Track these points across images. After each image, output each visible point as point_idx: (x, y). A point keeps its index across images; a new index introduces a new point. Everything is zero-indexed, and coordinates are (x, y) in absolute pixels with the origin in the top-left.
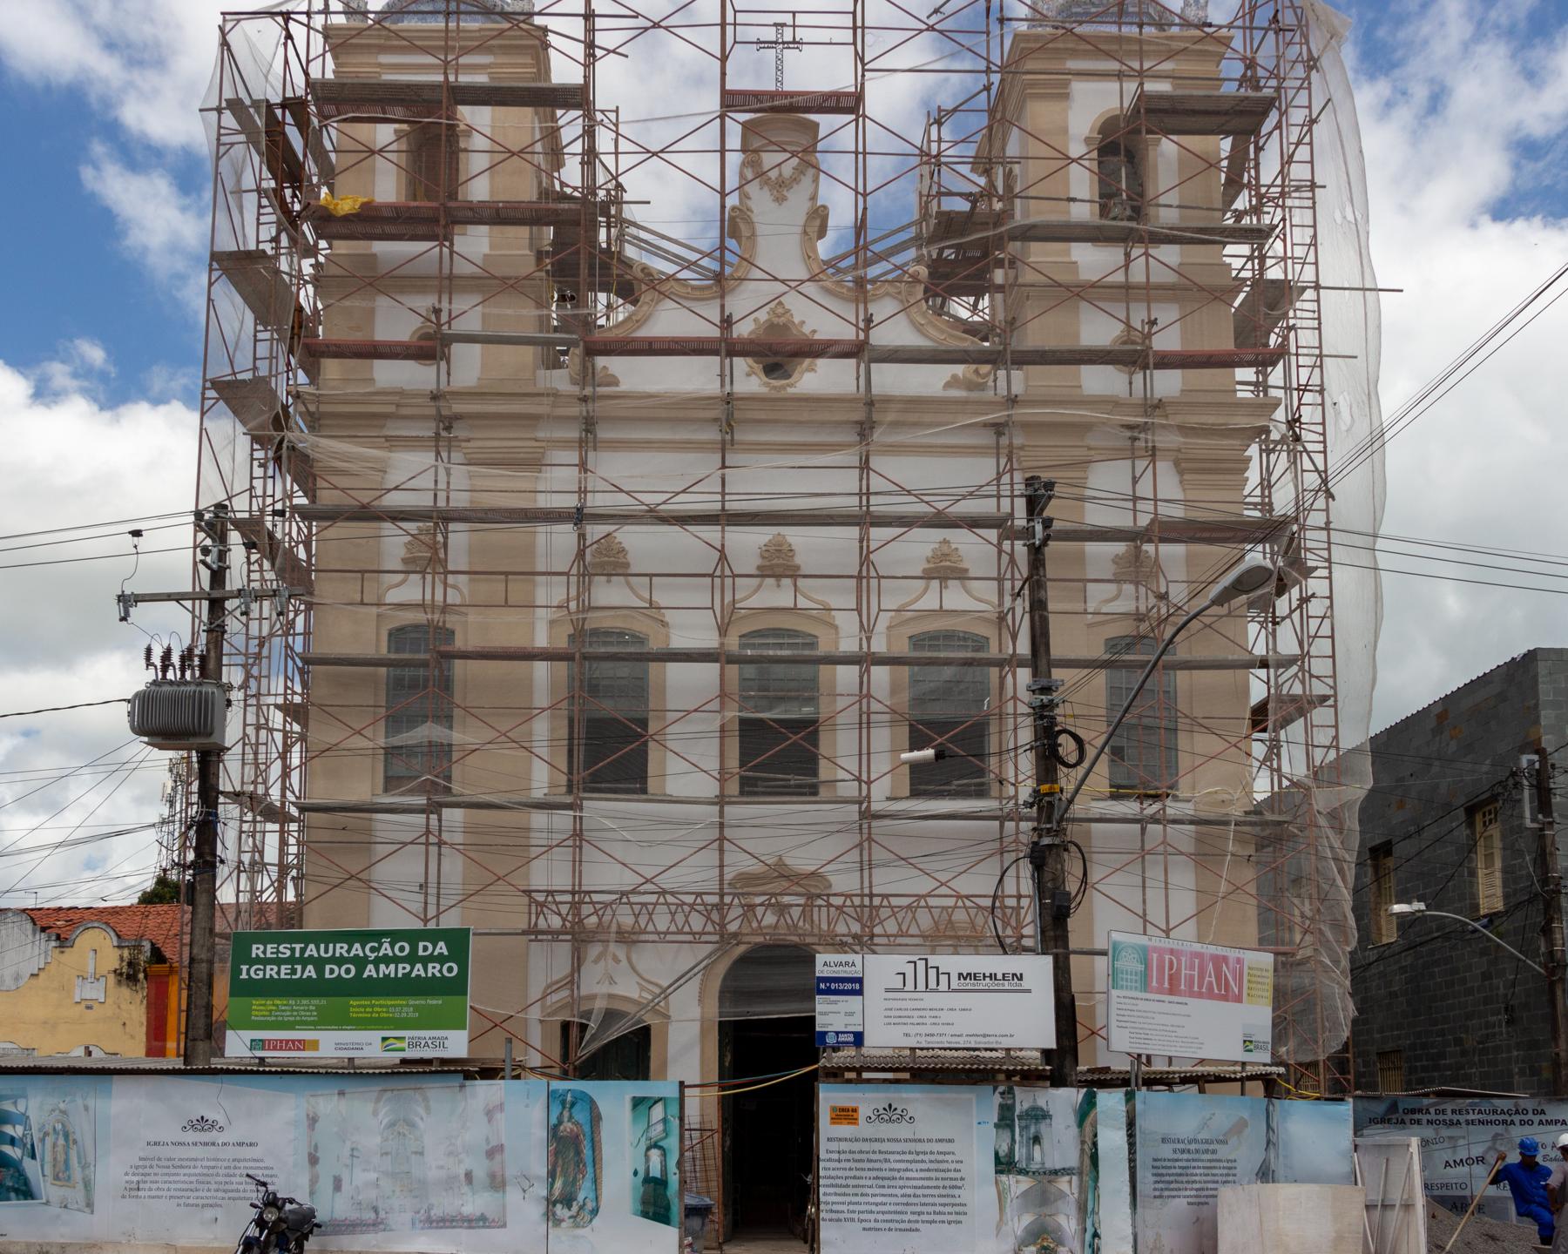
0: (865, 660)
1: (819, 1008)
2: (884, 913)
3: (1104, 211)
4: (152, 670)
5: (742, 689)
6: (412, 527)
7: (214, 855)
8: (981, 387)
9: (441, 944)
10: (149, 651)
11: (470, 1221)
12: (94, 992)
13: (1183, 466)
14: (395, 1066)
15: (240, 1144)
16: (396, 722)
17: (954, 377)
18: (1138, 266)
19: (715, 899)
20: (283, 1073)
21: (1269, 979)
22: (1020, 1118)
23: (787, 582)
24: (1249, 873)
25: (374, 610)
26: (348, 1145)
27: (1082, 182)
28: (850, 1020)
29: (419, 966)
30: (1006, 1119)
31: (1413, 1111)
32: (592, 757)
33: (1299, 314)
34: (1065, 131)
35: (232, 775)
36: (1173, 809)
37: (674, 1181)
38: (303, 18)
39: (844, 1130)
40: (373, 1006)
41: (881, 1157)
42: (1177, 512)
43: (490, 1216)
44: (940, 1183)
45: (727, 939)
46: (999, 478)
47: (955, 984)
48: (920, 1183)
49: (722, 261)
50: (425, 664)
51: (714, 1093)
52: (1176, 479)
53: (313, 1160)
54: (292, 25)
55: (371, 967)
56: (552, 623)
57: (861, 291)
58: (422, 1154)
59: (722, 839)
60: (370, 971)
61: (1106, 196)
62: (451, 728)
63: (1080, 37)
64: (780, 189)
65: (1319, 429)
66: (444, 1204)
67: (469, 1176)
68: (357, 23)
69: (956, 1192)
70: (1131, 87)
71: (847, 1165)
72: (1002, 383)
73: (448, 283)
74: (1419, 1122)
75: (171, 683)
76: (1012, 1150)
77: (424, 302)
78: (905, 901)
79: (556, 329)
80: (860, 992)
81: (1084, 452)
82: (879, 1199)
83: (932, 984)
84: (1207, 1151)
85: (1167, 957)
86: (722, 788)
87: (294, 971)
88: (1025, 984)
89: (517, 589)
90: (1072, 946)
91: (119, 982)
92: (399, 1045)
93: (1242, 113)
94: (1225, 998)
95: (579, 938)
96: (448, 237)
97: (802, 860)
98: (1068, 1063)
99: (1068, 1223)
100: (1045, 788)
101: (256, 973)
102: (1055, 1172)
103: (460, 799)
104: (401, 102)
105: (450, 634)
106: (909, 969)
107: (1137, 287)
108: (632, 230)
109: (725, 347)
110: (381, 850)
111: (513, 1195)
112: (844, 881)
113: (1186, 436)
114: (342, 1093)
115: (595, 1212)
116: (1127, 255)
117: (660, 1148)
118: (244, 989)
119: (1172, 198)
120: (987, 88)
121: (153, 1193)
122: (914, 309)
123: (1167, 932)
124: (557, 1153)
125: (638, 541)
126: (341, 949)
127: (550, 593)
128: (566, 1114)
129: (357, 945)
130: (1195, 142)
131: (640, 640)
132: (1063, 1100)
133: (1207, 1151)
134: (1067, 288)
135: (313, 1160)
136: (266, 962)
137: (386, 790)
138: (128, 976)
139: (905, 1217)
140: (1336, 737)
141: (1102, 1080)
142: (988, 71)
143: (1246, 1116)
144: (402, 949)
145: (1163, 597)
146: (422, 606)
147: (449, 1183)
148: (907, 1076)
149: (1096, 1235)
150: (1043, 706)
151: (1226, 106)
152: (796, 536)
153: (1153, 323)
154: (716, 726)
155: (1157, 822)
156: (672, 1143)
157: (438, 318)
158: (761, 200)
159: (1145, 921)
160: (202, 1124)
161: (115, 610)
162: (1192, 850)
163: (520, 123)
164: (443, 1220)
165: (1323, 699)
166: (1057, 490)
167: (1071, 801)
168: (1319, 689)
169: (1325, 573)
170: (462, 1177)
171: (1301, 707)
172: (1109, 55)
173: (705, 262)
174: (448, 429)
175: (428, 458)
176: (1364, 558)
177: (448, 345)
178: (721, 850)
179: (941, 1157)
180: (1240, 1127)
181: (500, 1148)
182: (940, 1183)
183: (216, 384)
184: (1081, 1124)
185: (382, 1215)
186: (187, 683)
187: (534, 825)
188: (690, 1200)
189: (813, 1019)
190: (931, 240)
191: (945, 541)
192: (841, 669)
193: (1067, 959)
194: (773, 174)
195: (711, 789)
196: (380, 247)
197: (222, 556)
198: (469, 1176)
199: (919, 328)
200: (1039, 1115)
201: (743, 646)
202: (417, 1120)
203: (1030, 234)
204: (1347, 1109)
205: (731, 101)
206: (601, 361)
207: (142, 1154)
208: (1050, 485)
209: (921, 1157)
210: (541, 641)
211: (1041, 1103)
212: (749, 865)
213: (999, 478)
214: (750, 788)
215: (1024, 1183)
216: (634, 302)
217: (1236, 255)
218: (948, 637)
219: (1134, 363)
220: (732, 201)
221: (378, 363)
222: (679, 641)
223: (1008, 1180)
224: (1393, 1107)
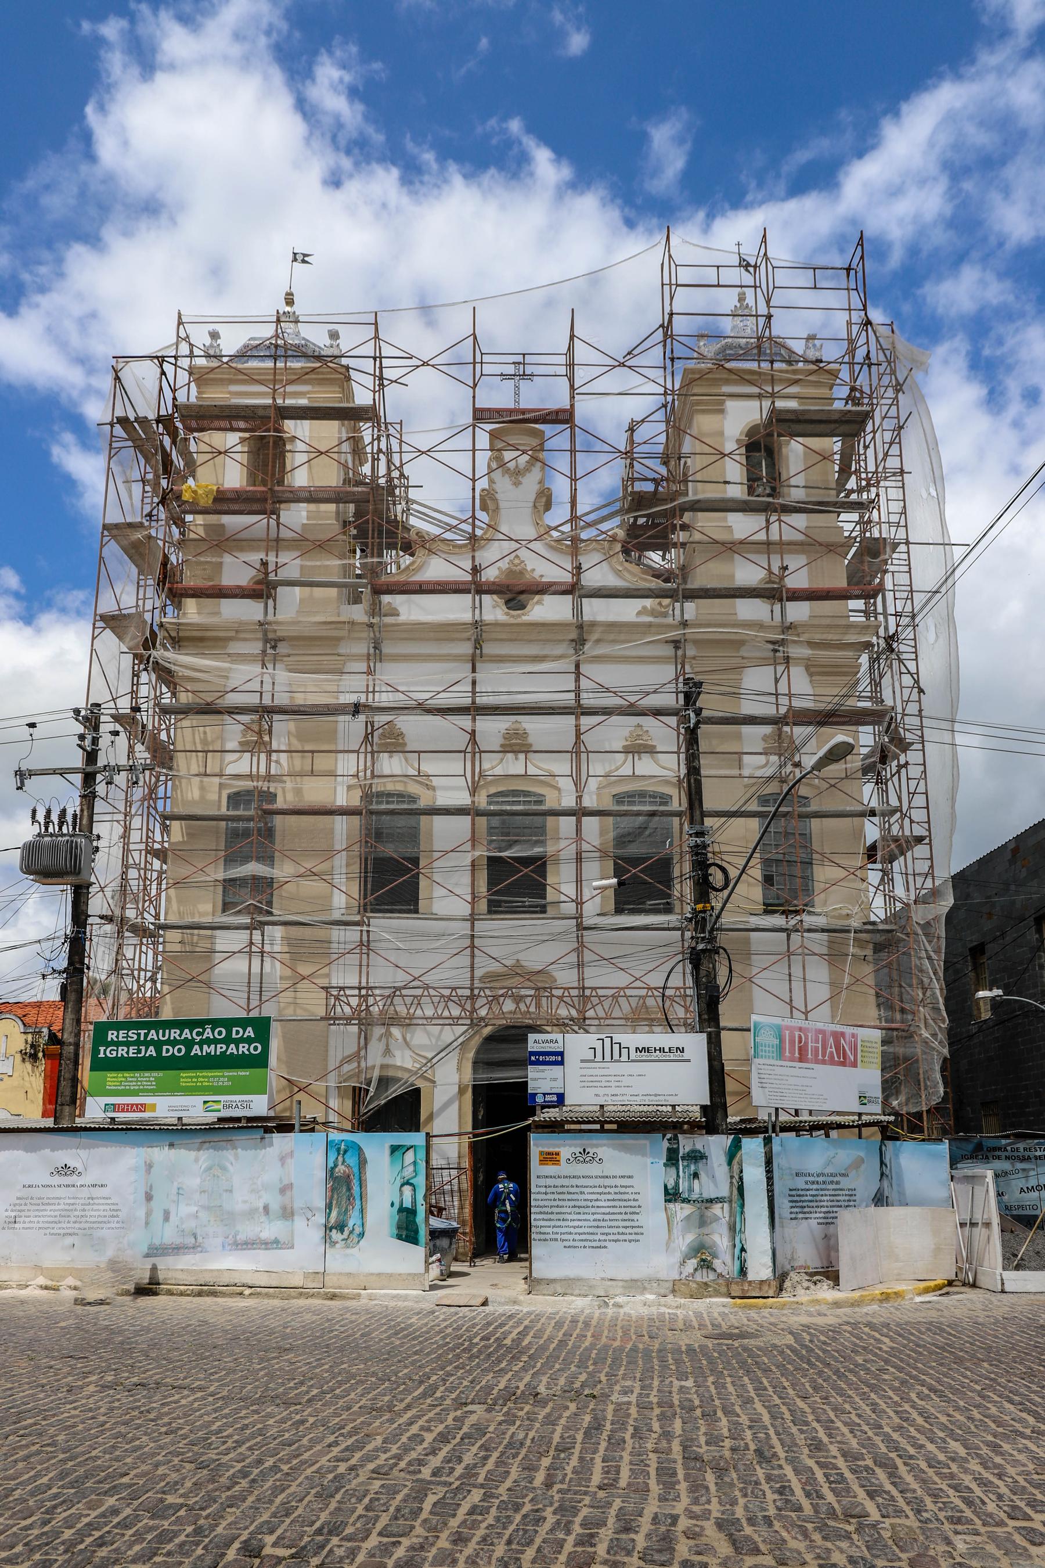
0: (579, 813)
1: (530, 1075)
2: (595, 1000)
3: (751, 491)
4: (36, 825)
5: (490, 834)
6: (245, 718)
7: (83, 963)
8: (665, 615)
9: (250, 1029)
10: (34, 812)
11: (266, 1244)
12: (5, 1067)
13: (813, 669)
14: (213, 1123)
15: (94, 1186)
16: (230, 860)
17: (644, 608)
18: (775, 527)
19: (467, 992)
20: (127, 1129)
21: (879, 1048)
22: (683, 1158)
23: (522, 756)
24: (869, 969)
25: (217, 780)
26: (176, 1185)
27: (735, 470)
28: (554, 1084)
29: (232, 1046)
30: (672, 1158)
31: (995, 1149)
32: (377, 885)
33: (895, 562)
34: (721, 434)
35: (97, 905)
36: (808, 920)
37: (421, 1211)
38: (172, 360)
39: (550, 1169)
40: (197, 1077)
41: (578, 1190)
42: (808, 704)
43: (282, 1240)
44: (623, 1210)
45: (475, 1023)
46: (677, 679)
47: (633, 1055)
48: (607, 1210)
49: (474, 526)
50: (249, 819)
51: (466, 1140)
52: (808, 679)
53: (149, 1197)
54: (165, 365)
55: (196, 1047)
56: (350, 788)
57: (575, 546)
58: (231, 1191)
59: (473, 947)
60: (196, 1050)
61: (752, 479)
62: (272, 866)
63: (730, 370)
64: (517, 475)
65: (912, 643)
66: (247, 1230)
67: (266, 1209)
68: (215, 363)
69: (635, 1217)
70: (766, 404)
71: (552, 1197)
72: (677, 612)
73: (277, 544)
74: (999, 1158)
75: (51, 835)
76: (677, 1184)
77: (255, 557)
78: (610, 992)
79: (359, 576)
80: (561, 1063)
81: (739, 660)
82: (576, 1223)
83: (616, 1056)
84: (832, 1182)
85: (797, 1034)
86: (473, 908)
87: (139, 1051)
88: (686, 1055)
89: (322, 762)
90: (722, 1024)
91: (24, 1060)
92: (216, 1107)
93: (847, 422)
94: (843, 1064)
95: (364, 1021)
96: (275, 512)
97: (535, 959)
98: (719, 1115)
99: (721, 1240)
100: (700, 907)
101: (111, 1053)
102: (711, 1201)
103: (281, 919)
104: (244, 418)
105: (272, 797)
106: (598, 1045)
107: (775, 543)
108: (415, 506)
109: (477, 588)
110: (218, 957)
111: (299, 1223)
112: (566, 977)
113: (812, 648)
114: (171, 1145)
115: (362, 1235)
116: (768, 521)
117: (411, 1184)
118: (100, 1065)
119: (799, 480)
120: (665, 406)
121: (27, 1225)
122: (614, 559)
123: (806, 1013)
124: (333, 1190)
125: (412, 726)
126: (175, 1034)
127: (348, 764)
128: (340, 1159)
129: (187, 1031)
130: (815, 443)
131: (413, 799)
132: (716, 1145)
133: (832, 1182)
134: (723, 544)
135: (149, 1197)
136: (117, 1044)
137: (224, 911)
138: (31, 1055)
139: (597, 1237)
140: (932, 867)
141: (749, 1128)
142: (665, 394)
143: (862, 1154)
144: (220, 1033)
145: (797, 765)
146: (250, 776)
147: (251, 1213)
148: (567, 1127)
149: (743, 1250)
150: (697, 846)
151: (836, 417)
152: (532, 725)
153: (786, 568)
154: (468, 861)
155: (797, 931)
156: (420, 1181)
157: (266, 569)
158: (503, 484)
159: (792, 1007)
160: (66, 1170)
161: (13, 782)
162: (825, 951)
163: (330, 431)
164: (246, 1243)
165: (919, 840)
166: (705, 688)
167: (718, 917)
168: (919, 831)
169: (920, 746)
170: (261, 1209)
171: (901, 846)
172: (751, 383)
173: (463, 526)
174: (274, 647)
175: (257, 669)
176: (947, 737)
177: (275, 588)
178: (473, 956)
179: (623, 1190)
180: (858, 1163)
181: (290, 1186)
182: (623, 1210)
183: (103, 618)
184: (730, 1163)
185: (200, 1239)
186: (63, 835)
187: (334, 938)
188: (436, 1223)
189: (525, 1084)
190: (629, 510)
191: (639, 726)
192: (562, 819)
193: (718, 1035)
194: (512, 465)
195: (466, 910)
196: (226, 519)
197: (95, 741)
198: (266, 1209)
199: (618, 573)
200: (697, 1156)
201: (489, 803)
202: (228, 1165)
203: (698, 506)
204: (944, 1147)
205: (480, 415)
206: (386, 599)
207: (19, 1195)
208: (699, 685)
209: (608, 1190)
210: (342, 799)
211: (699, 1147)
212: (495, 967)
213: (677, 679)
214: (495, 908)
215: (687, 1209)
216: (412, 555)
217: (848, 522)
218: (642, 794)
219: (773, 597)
220: (482, 484)
221: (224, 602)
222: (443, 799)
223: (676, 1207)
224: (979, 1147)
